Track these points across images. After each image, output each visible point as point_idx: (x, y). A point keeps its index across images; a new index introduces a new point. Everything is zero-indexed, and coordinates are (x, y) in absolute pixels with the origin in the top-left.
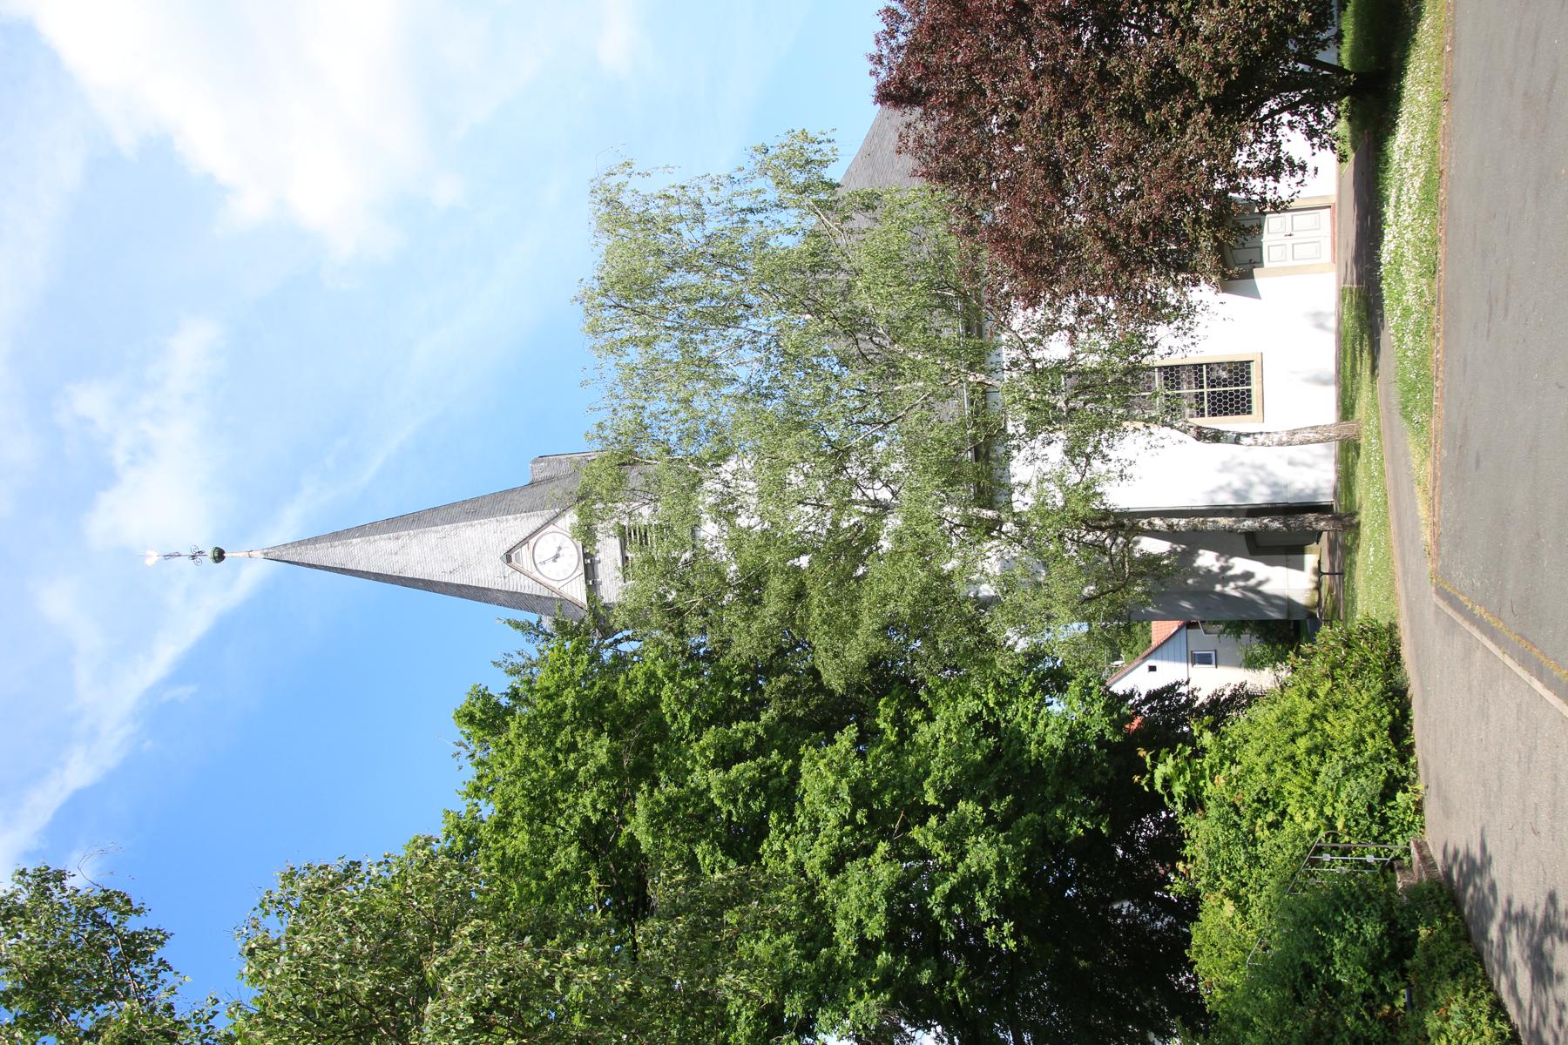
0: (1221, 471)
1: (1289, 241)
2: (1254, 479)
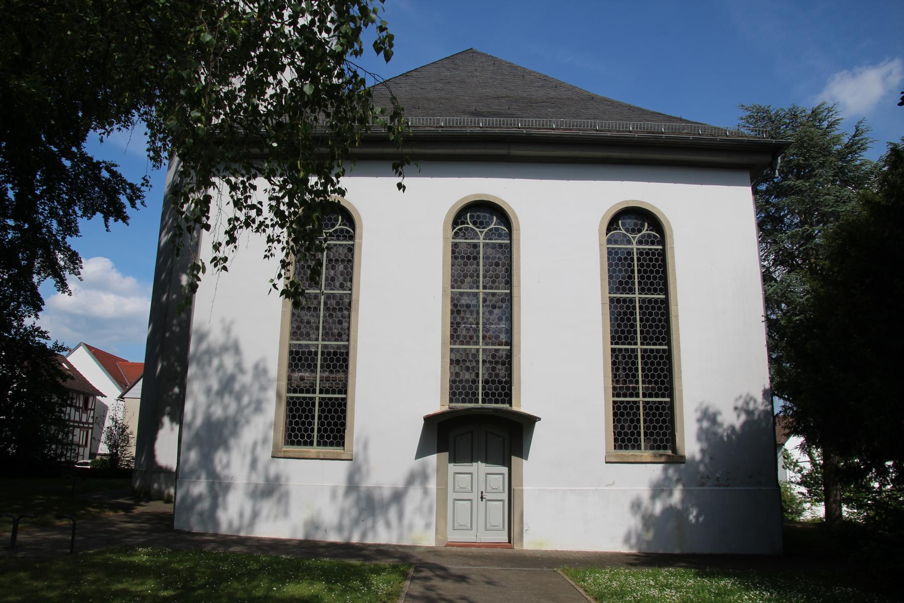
0: (256, 367)
1: (475, 496)
2: (245, 400)
